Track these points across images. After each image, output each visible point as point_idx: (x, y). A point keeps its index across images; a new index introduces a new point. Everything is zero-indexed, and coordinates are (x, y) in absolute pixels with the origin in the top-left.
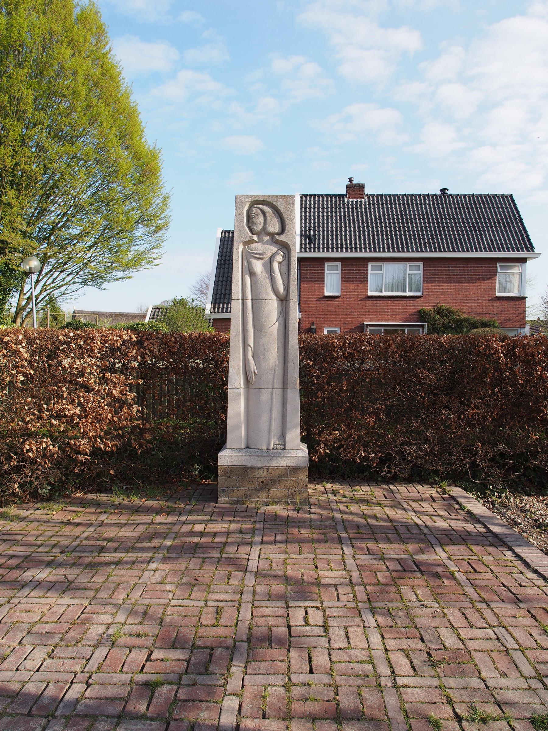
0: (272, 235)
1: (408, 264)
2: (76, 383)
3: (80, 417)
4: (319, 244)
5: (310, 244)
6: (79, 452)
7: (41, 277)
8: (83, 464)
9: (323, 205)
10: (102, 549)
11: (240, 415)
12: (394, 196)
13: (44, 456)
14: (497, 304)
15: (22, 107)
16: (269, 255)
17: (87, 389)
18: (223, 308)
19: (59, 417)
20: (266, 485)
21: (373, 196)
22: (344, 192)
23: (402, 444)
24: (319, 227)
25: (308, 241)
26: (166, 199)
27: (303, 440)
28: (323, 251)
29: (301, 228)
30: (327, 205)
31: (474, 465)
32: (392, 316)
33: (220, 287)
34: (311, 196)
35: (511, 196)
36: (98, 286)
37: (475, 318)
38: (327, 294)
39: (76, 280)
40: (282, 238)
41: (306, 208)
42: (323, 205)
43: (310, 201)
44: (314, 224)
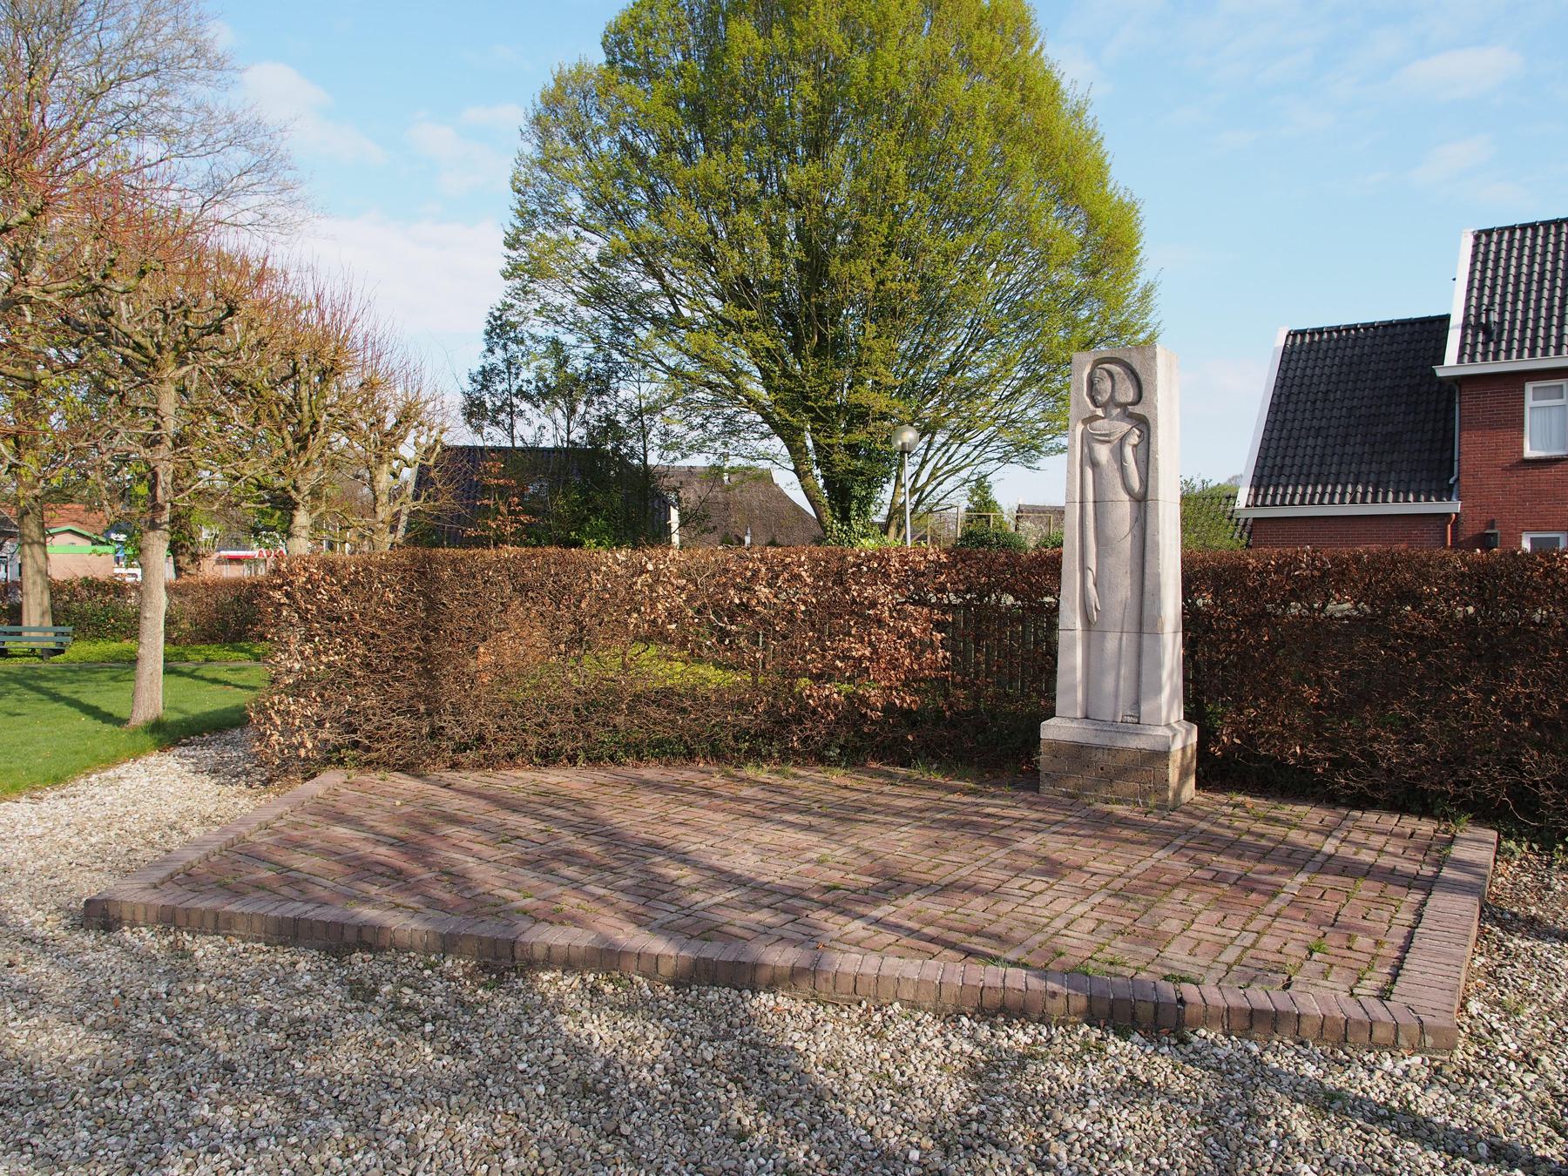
0: (1124, 406)
2: (862, 613)
3: (871, 660)
4: (1510, 342)
5: (1485, 344)
6: (868, 706)
7: (931, 452)
8: (873, 722)
9: (1533, 247)
10: (863, 810)
11: (1075, 668)
13: (827, 706)
15: (890, 191)
16: (1119, 435)
17: (880, 622)
18: (1274, 496)
19: (844, 658)
20: (1110, 777)
23: (1374, 738)
24: (1514, 303)
25: (1481, 338)
26: (1145, 295)
27: (1189, 717)
28: (1520, 355)
29: (1467, 308)
30: (1545, 245)
33: (1272, 452)
36: (1028, 463)
38: (1529, 453)
39: (990, 455)
40: (1137, 410)
41: (1485, 262)
42: (1533, 247)
43: (1499, 243)
44: (1503, 296)
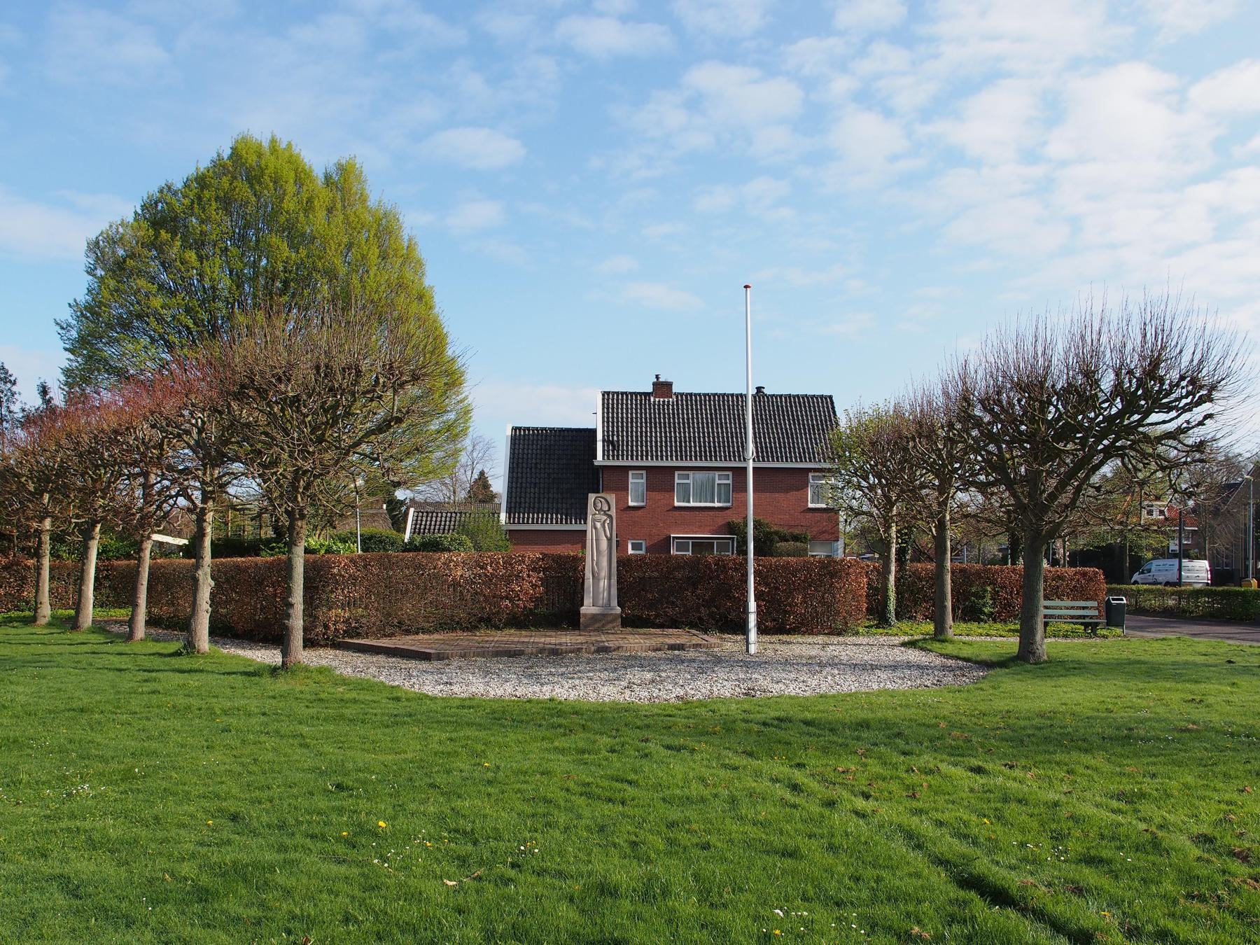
1: (717, 473)
12: (705, 395)
14: (809, 515)
21: (682, 395)
22: (650, 390)
31: (700, 618)
32: (701, 529)
34: (614, 393)
35: (831, 397)
37: (785, 531)
